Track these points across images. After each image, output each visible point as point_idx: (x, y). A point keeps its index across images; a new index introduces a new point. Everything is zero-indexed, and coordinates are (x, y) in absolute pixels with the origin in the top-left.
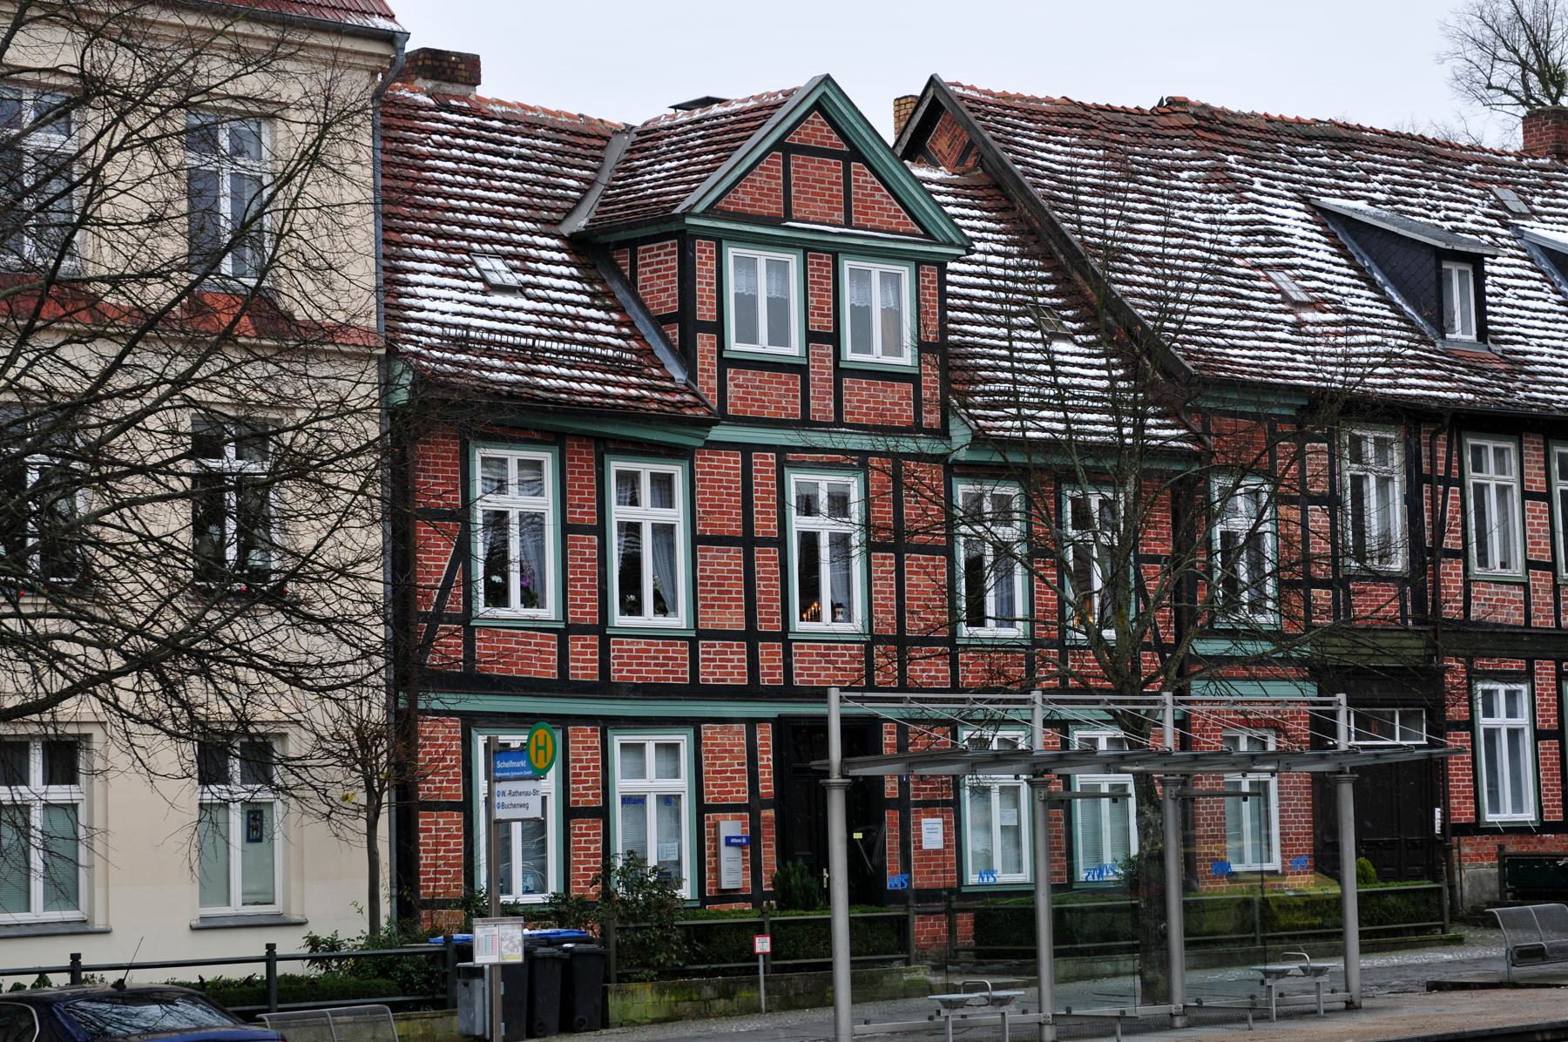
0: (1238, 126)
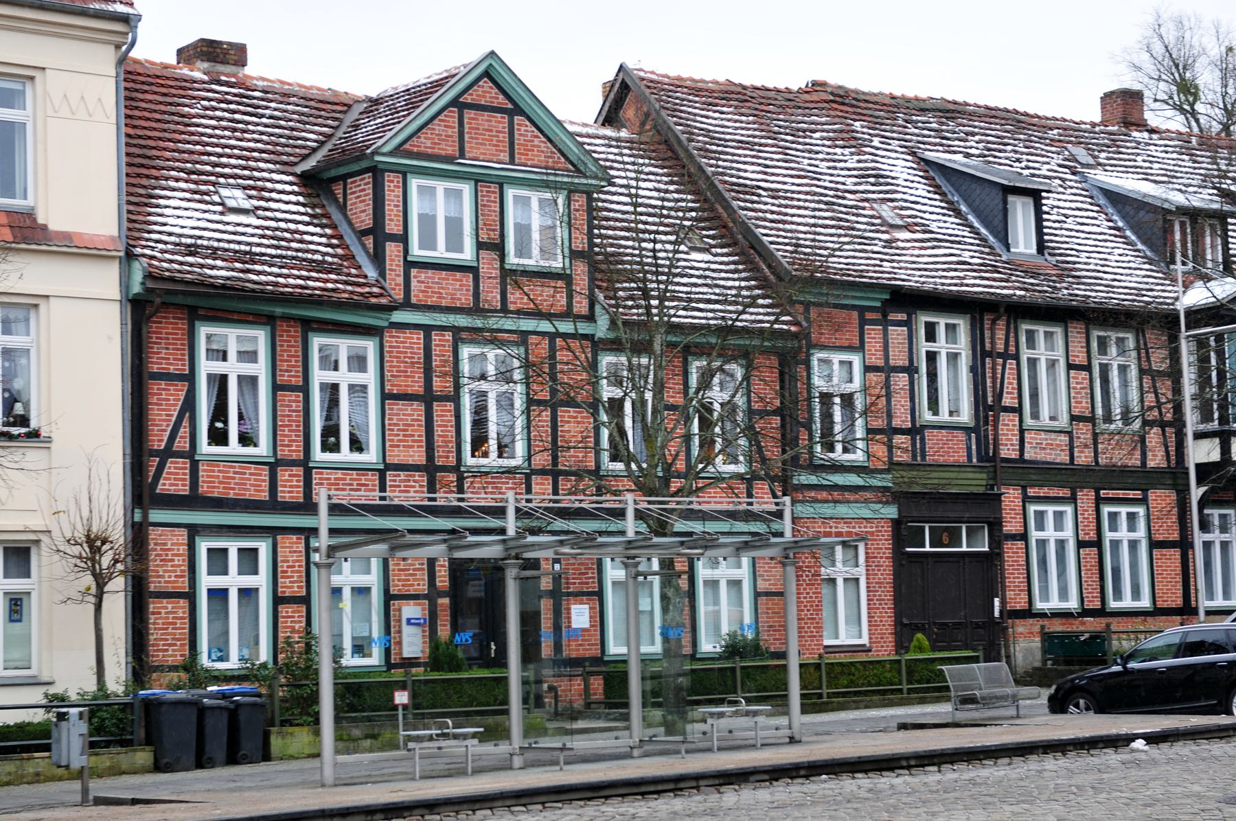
0: (866, 101)
